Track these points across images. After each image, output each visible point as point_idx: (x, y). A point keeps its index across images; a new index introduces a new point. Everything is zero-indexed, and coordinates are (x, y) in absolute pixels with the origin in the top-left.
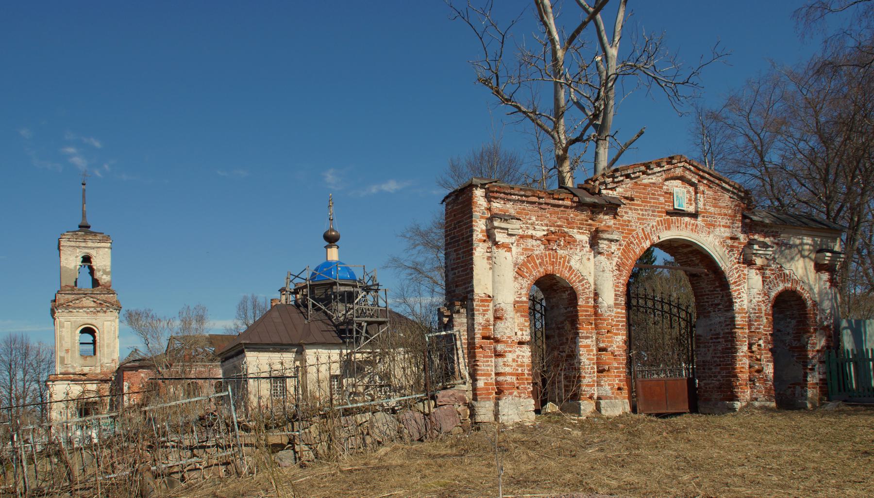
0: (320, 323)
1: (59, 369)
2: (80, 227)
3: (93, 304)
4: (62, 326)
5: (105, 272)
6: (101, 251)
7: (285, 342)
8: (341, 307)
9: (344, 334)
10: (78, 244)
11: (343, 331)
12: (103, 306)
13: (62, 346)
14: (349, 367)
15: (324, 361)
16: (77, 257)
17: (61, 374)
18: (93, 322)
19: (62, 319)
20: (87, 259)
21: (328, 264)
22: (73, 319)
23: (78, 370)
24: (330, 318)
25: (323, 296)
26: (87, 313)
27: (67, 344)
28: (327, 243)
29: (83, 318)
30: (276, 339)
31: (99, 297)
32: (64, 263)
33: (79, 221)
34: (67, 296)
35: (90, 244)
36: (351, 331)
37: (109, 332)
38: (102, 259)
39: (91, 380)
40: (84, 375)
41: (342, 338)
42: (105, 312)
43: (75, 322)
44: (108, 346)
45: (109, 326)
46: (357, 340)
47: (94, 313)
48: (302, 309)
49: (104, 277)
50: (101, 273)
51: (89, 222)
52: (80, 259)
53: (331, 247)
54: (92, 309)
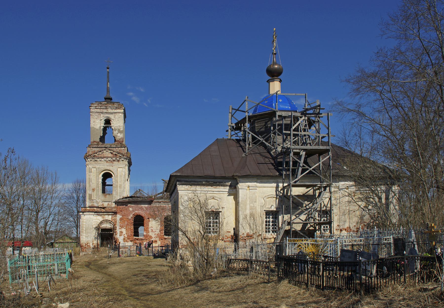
0: (258, 156)
1: (88, 204)
2: (105, 99)
3: (110, 155)
4: (90, 172)
5: (120, 131)
6: (117, 116)
7: (217, 175)
8: (279, 139)
9: (279, 167)
10: (102, 110)
11: (281, 164)
12: (117, 157)
13: (90, 186)
14: (287, 203)
15: (260, 195)
16: (101, 120)
17: (89, 207)
18: (111, 168)
19: (90, 166)
20: (108, 122)
21: (272, 98)
22: (97, 166)
23: (100, 204)
24: (269, 150)
25: (263, 130)
26: (107, 162)
27: (94, 186)
28: (270, 78)
29: (105, 165)
30: (209, 172)
31: (115, 149)
32: (92, 125)
33: (105, 95)
34: (94, 149)
35: (110, 110)
36: (288, 163)
37: (121, 176)
38: (118, 122)
39: (107, 212)
40: (104, 208)
41: (279, 171)
42: (118, 161)
43: (99, 168)
44: (120, 187)
45: (120, 170)
46: (294, 173)
47: (111, 162)
48: (242, 143)
49: (119, 135)
50: (117, 132)
51: (111, 96)
52: (103, 122)
53: (273, 80)
54: (110, 159)
